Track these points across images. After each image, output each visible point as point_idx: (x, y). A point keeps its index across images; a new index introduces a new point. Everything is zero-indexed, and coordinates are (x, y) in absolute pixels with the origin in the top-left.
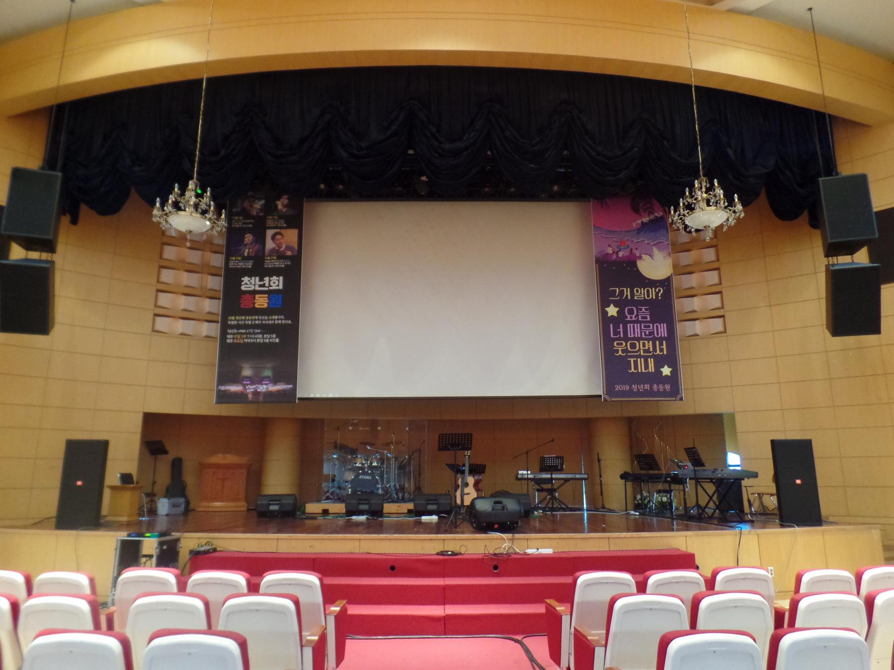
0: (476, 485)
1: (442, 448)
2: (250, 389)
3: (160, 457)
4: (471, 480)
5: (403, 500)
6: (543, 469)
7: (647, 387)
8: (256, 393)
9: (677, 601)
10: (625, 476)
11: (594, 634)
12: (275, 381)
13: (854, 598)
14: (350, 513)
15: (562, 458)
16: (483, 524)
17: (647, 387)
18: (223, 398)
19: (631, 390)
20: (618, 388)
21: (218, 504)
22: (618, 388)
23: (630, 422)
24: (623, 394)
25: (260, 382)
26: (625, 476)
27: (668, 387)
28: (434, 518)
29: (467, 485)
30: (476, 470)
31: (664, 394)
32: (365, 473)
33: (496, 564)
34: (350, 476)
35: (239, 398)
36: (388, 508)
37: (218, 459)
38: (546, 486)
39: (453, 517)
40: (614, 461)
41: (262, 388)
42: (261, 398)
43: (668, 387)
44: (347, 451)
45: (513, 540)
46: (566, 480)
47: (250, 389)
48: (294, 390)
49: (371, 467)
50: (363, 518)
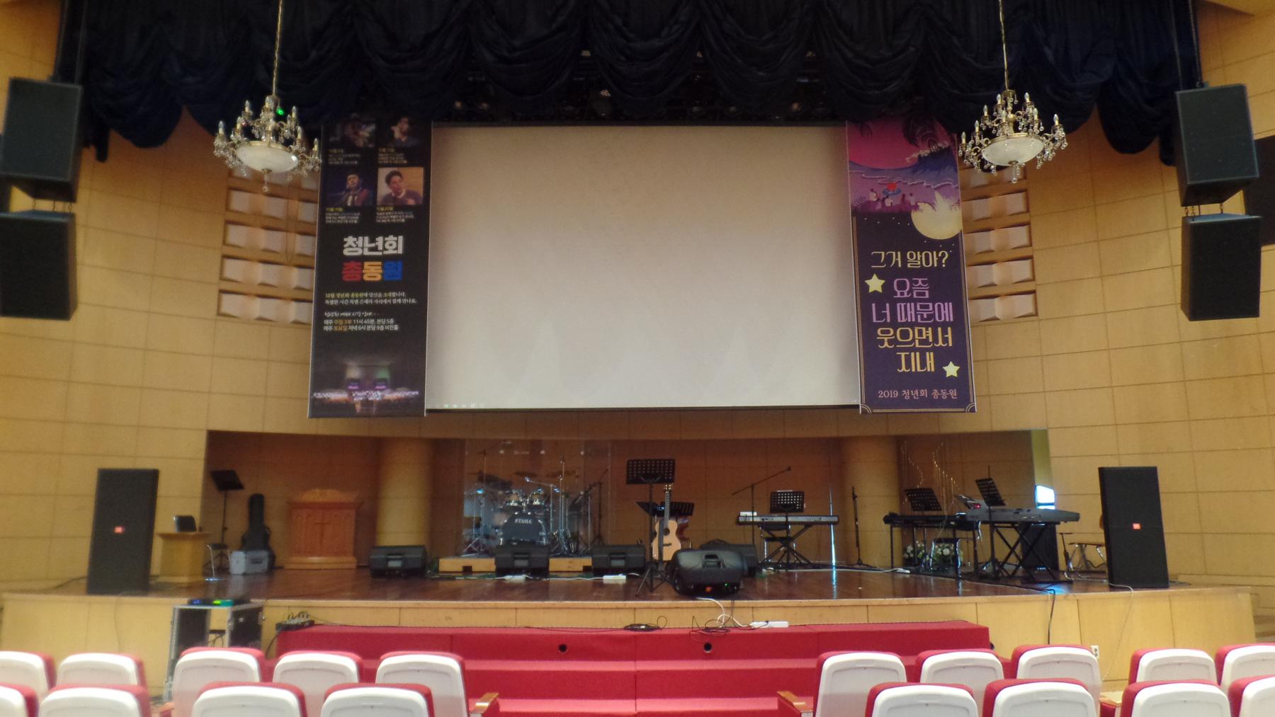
0: (680, 532)
1: (632, 480)
2: (359, 397)
3: (232, 493)
4: (673, 525)
5: (577, 554)
6: (775, 509)
7: (924, 393)
8: (366, 403)
12: (394, 386)
14: (502, 571)
15: (802, 494)
17: (924, 393)
18: (321, 409)
19: (901, 397)
20: (882, 394)
21: (315, 559)
22: (882, 394)
23: (899, 443)
27: (953, 393)
28: (621, 578)
29: (667, 532)
30: (680, 510)
31: (949, 403)
32: (525, 516)
33: (709, 642)
36: (556, 564)
37: (315, 496)
39: (648, 577)
40: (876, 497)
41: (376, 396)
42: (374, 409)
43: (953, 393)
45: (732, 608)
46: (808, 525)
47: (359, 397)
48: (421, 399)
50: (520, 578)
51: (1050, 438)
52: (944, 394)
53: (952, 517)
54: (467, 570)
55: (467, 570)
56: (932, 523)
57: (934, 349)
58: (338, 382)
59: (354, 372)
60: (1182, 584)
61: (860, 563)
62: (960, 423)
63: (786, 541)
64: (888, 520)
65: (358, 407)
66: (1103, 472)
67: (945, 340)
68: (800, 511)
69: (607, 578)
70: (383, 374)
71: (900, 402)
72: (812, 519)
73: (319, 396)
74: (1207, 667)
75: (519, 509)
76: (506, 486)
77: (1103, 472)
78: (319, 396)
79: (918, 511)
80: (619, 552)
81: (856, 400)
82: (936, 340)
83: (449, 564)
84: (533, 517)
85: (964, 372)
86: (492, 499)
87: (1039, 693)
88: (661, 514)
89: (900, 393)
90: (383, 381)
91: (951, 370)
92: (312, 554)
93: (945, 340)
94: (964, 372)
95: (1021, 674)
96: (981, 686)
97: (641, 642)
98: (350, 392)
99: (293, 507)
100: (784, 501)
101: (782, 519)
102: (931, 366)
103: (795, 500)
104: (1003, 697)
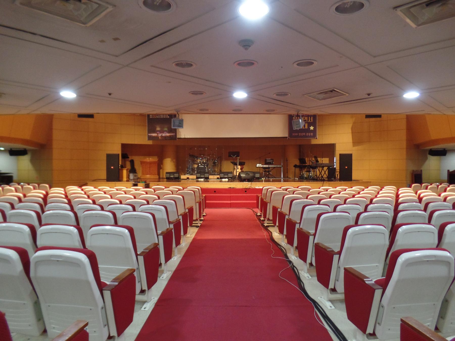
0: (241, 169)
2: (160, 135)
5: (215, 175)
8: (162, 136)
10: (295, 166)
12: (169, 132)
14: (197, 178)
15: (273, 160)
16: (241, 180)
17: (304, 134)
19: (298, 135)
20: (293, 134)
22: (293, 134)
23: (300, 146)
24: (295, 137)
26: (295, 166)
27: (312, 134)
30: (242, 164)
31: (311, 136)
32: (201, 165)
34: (196, 166)
39: (232, 179)
41: (164, 135)
47: (160, 135)
48: (176, 135)
49: (203, 163)
50: (202, 180)
51: (125, 143)
52: (309, 134)
54: (188, 178)
55: (188, 178)
56: (305, 167)
57: (307, 123)
58: (154, 131)
59: (158, 129)
61: (287, 177)
63: (269, 171)
65: (160, 138)
66: (340, 154)
67: (311, 120)
68: (272, 164)
69: (223, 180)
70: (166, 129)
72: (275, 166)
73: (150, 135)
76: (197, 157)
77: (340, 154)
78: (150, 135)
79: (302, 165)
80: (227, 173)
81: (287, 136)
82: (308, 120)
83: (183, 177)
84: (204, 165)
85: (315, 129)
87: (374, 215)
88: (236, 165)
89: (306, 134)
90: (166, 131)
91: (312, 128)
92: (147, 175)
93: (311, 120)
94: (315, 129)
95: (368, 210)
96: (358, 212)
98: (158, 134)
99: (142, 163)
100: (268, 161)
101: (268, 166)
102: (306, 127)
103: (271, 161)
104: (362, 216)
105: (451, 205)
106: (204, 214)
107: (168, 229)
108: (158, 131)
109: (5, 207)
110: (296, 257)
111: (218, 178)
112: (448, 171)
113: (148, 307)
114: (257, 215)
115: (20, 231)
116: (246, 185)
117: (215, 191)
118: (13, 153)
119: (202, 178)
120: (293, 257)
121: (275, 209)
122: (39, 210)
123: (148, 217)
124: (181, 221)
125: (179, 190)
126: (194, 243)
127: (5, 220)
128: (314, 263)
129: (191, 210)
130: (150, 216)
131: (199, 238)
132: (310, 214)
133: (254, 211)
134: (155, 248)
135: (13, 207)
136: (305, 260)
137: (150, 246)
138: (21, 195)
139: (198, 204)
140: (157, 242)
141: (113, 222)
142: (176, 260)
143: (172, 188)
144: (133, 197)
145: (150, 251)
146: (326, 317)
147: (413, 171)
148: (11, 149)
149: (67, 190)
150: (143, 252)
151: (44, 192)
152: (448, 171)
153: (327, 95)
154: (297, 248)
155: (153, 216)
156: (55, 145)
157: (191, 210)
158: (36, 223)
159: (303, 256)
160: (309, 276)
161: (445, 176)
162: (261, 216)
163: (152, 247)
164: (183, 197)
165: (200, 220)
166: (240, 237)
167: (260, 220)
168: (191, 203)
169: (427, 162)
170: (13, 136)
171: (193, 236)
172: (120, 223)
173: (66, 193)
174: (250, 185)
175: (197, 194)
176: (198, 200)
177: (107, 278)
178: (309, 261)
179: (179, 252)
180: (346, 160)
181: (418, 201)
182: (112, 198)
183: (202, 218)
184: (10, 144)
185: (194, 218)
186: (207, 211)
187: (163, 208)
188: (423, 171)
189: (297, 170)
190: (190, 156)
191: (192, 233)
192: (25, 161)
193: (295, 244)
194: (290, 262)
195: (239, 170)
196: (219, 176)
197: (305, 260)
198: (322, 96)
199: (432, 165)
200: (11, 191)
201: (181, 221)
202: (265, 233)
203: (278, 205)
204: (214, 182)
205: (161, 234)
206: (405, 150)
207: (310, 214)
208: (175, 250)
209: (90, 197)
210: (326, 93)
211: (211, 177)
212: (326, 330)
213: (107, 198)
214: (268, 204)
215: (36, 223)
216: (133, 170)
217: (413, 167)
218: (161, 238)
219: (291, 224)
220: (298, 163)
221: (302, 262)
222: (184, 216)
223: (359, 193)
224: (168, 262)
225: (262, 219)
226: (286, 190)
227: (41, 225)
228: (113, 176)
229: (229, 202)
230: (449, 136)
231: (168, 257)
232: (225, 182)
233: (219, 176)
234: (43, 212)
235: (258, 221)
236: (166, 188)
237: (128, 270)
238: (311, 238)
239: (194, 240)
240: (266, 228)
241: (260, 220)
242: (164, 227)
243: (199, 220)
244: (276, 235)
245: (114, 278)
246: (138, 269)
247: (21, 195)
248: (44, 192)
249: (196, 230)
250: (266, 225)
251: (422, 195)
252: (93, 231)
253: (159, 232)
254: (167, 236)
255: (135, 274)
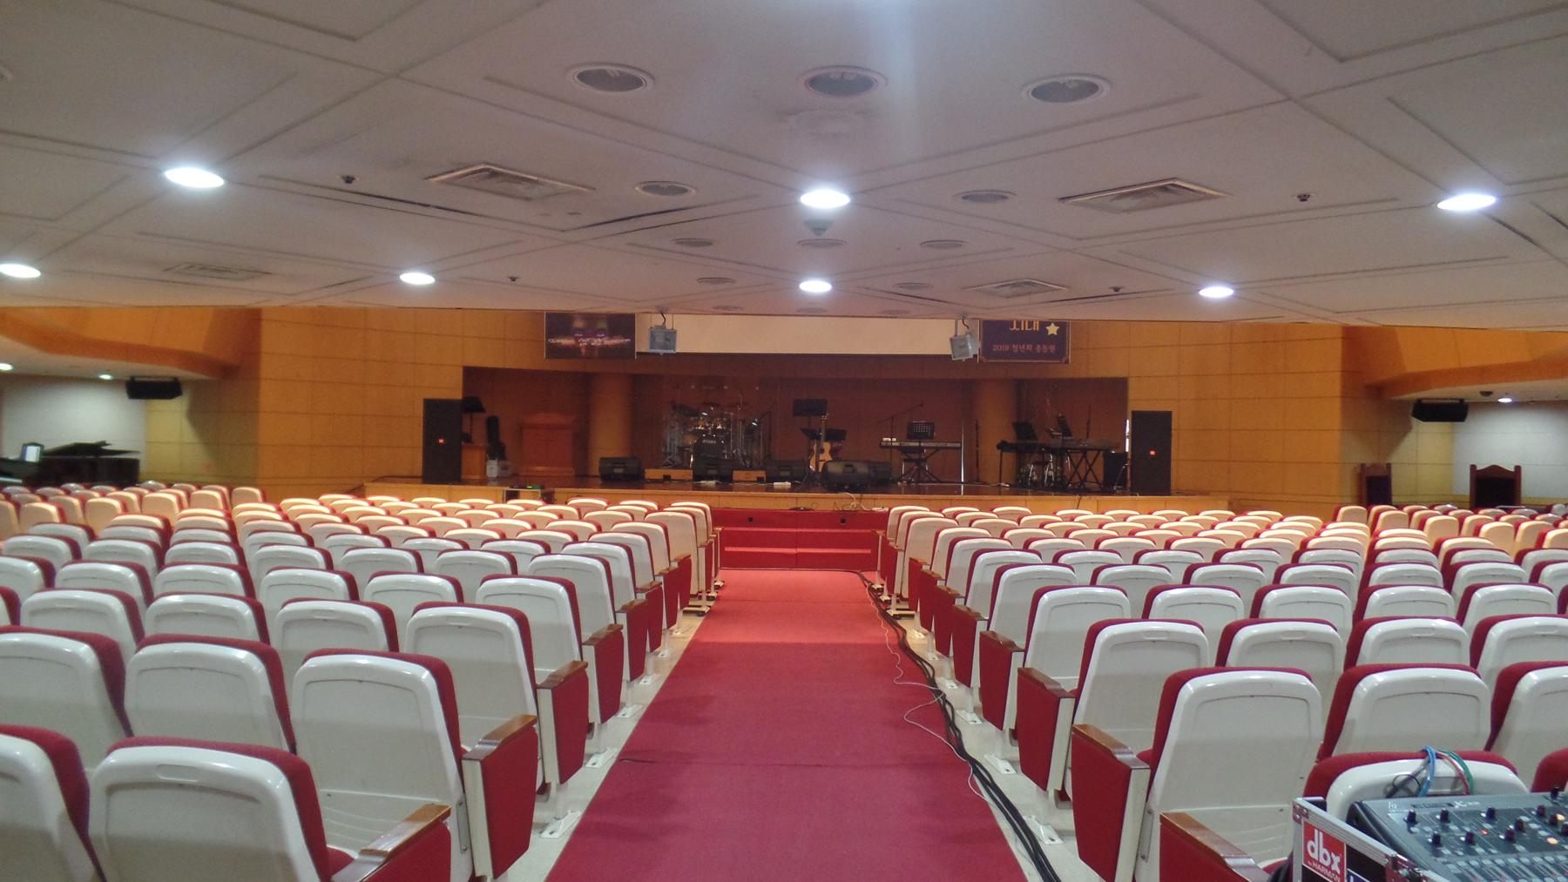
0: (832, 452)
1: (796, 413)
2: (584, 342)
3: (476, 415)
4: (827, 446)
5: (751, 468)
6: (911, 437)
7: (1029, 347)
8: (590, 348)
9: (1303, 680)
10: (1003, 446)
11: (1131, 741)
12: (611, 334)
13: (1455, 626)
14: (697, 477)
15: (932, 425)
16: (833, 484)
17: (1029, 347)
18: (554, 352)
19: (1011, 350)
20: (996, 348)
21: (540, 468)
22: (996, 348)
23: (1019, 384)
24: (1001, 355)
25: (594, 335)
26: (1003, 446)
27: (1052, 348)
28: (788, 484)
29: (822, 451)
30: (833, 436)
31: (1048, 356)
32: (711, 438)
33: (843, 518)
34: (691, 441)
35: (571, 352)
36: (737, 475)
37: (539, 418)
38: (915, 456)
39: (803, 481)
40: (996, 426)
41: (597, 342)
42: (596, 354)
43: (1052, 348)
44: (688, 413)
45: (860, 499)
46: (937, 449)
47: (584, 342)
48: (632, 344)
49: (715, 430)
50: (712, 483)
53: (1042, 446)
54: (667, 478)
55: (667, 478)
60: (1179, 493)
62: (1066, 372)
64: (999, 447)
66: (1168, 415)
68: (931, 438)
69: (777, 484)
71: (1010, 354)
74: (1457, 643)
75: (705, 432)
77: (1168, 415)
86: (685, 425)
90: (602, 331)
97: (799, 517)
105: (1553, 598)
106: (719, 583)
107: (611, 627)
108: (579, 330)
109: (22, 575)
110: (1012, 763)
111: (760, 480)
112: (1473, 467)
113: (571, 820)
114: (871, 589)
115: (71, 662)
116: (845, 502)
117: (751, 518)
118: (140, 389)
119: (711, 478)
120: (948, 685)
121: (915, 565)
122: (136, 592)
123: (414, 680)
124: (625, 632)
125: (650, 511)
126: (694, 661)
127: (15, 625)
128: (1070, 794)
129: (685, 563)
130: (509, 622)
131: (706, 639)
132: (1064, 616)
133: (864, 579)
134: (615, 632)
135: (49, 576)
136: (999, 725)
137: (509, 725)
138: (79, 533)
139: (702, 551)
140: (533, 712)
141: (382, 642)
142: (599, 762)
143: (628, 504)
144: (528, 526)
145: (567, 678)
146: (991, 785)
147: (1363, 466)
148: (133, 378)
149: (236, 517)
150: (548, 681)
151: (158, 522)
152: (1473, 467)
153: (1150, 200)
154: (1014, 734)
155: (522, 620)
156: (269, 367)
157: (685, 563)
158: (122, 633)
159: (1035, 766)
160: (1055, 837)
161: (1464, 486)
162: (888, 603)
163: (516, 728)
164: (665, 529)
165: (709, 599)
166: (819, 640)
167: (877, 601)
168: (687, 545)
169: (1409, 441)
170: (157, 343)
171: (690, 636)
172: (405, 647)
173: (232, 525)
174: (855, 503)
175: (702, 524)
176: (703, 539)
177: (543, 671)
178: (1054, 783)
179: (656, 670)
180: (1155, 427)
181: (1440, 582)
182: (470, 526)
183: (713, 594)
184: (124, 364)
185: (693, 591)
186: (723, 577)
187: (622, 551)
188: (1394, 471)
189: (1009, 457)
190: (674, 407)
191: (682, 633)
192: (171, 416)
193: (1010, 720)
194: (939, 692)
195: (826, 456)
196: (762, 474)
197: (1042, 782)
198: (1007, 290)
199: (1426, 450)
200: (44, 518)
201: (625, 632)
202: (886, 634)
203: (923, 556)
204: (748, 489)
205: (592, 641)
206: (1337, 405)
207: (1064, 616)
208: (650, 661)
209: (317, 544)
210: (1014, 285)
211: (737, 475)
212: (985, 804)
213: (461, 527)
214: (900, 555)
215: (122, 633)
216: (496, 450)
217: (1362, 456)
218: (546, 696)
219: (998, 654)
220: (1011, 437)
221: (964, 687)
222: (670, 576)
223: (1239, 547)
224: (570, 781)
225: (885, 597)
226: (954, 516)
227: (141, 639)
228: (442, 467)
229: (793, 551)
230: (1451, 364)
231: (571, 762)
232: (783, 490)
233: (762, 474)
234: (149, 597)
235: (873, 606)
236: (609, 504)
237: (430, 808)
238: (1065, 706)
239: (694, 644)
240: (892, 621)
241: (877, 601)
242: (600, 618)
243: (704, 595)
244: (918, 637)
245: (495, 727)
246: (463, 803)
247: (79, 533)
248: (158, 522)
249: (697, 622)
250: (892, 612)
251: (1458, 558)
252: (311, 670)
253: (586, 635)
254: (568, 692)
255: (451, 824)
